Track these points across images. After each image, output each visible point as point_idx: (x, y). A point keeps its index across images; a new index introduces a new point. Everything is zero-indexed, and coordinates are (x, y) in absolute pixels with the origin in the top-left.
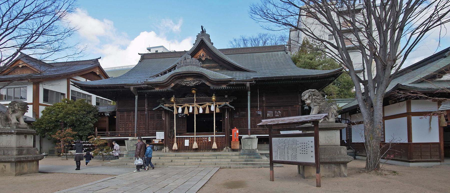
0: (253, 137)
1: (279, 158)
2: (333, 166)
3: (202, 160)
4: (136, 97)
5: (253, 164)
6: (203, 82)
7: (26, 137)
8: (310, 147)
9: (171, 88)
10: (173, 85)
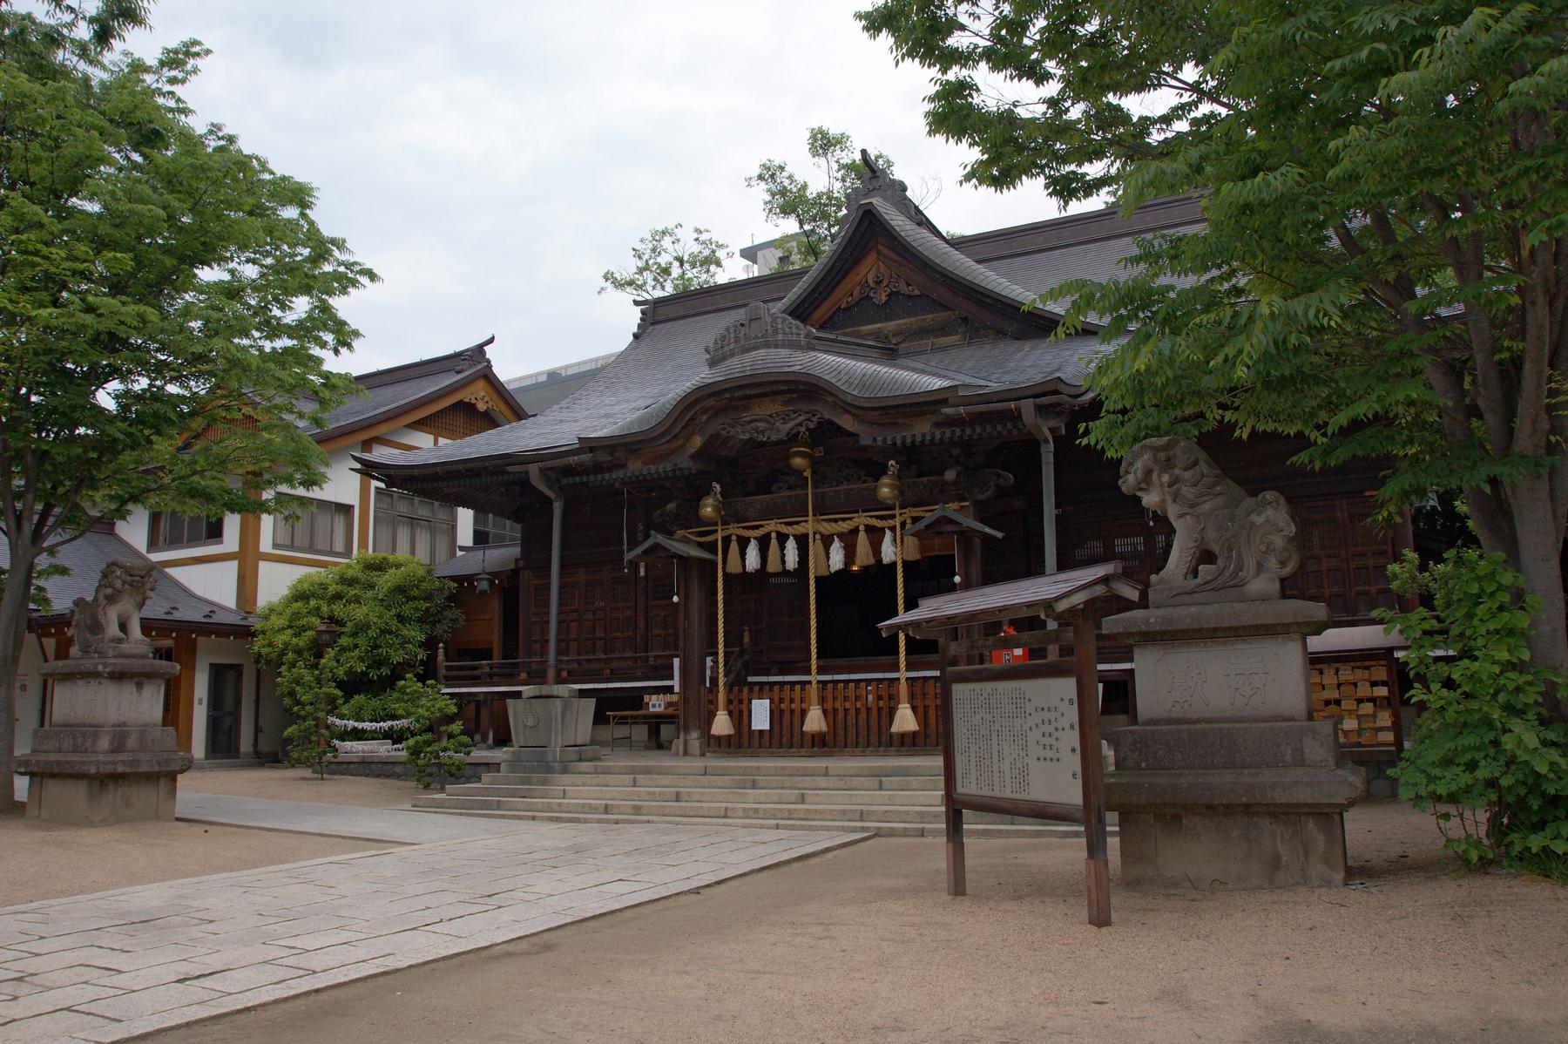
2: (1265, 823)
4: (557, 507)
6: (827, 416)
7: (140, 686)
8: (1067, 726)
9: (693, 457)
10: (697, 441)
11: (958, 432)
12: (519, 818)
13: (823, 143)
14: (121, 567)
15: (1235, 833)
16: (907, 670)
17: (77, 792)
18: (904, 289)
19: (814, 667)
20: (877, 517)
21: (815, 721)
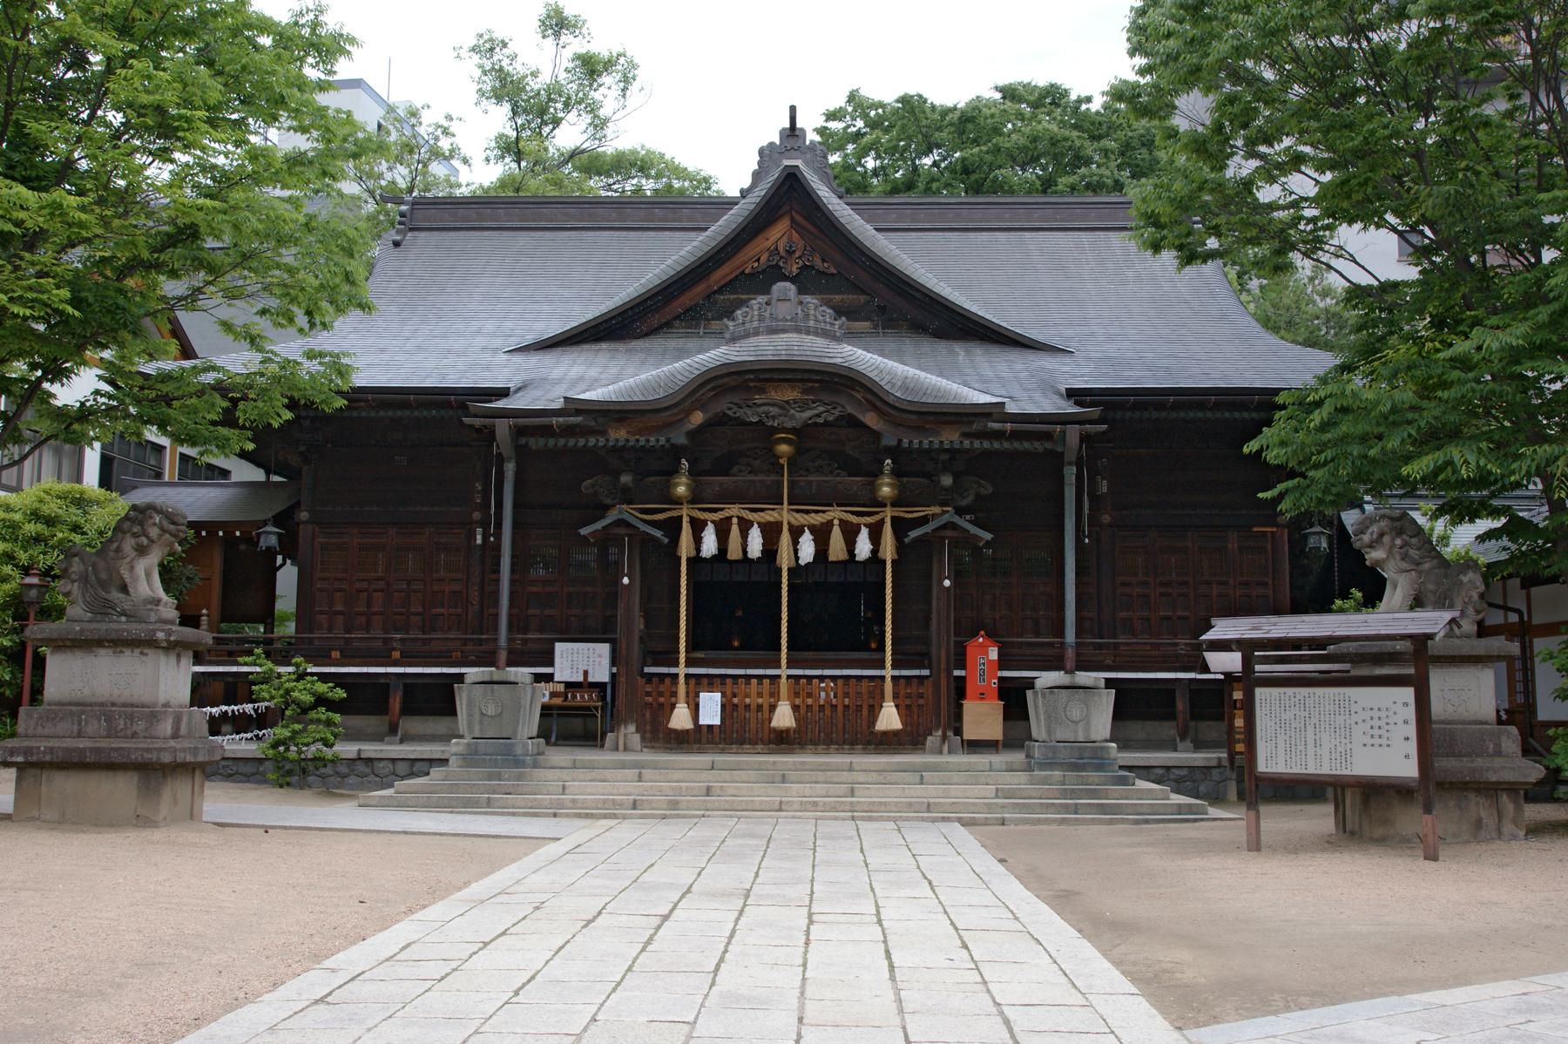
0: (1089, 683)
1: (1281, 760)
2: (1472, 796)
5: (1103, 809)
6: (850, 410)
7: (179, 656)
8: (1400, 722)
12: (514, 814)
13: (557, 24)
14: (159, 511)
15: (1452, 803)
17: (122, 788)
18: (818, 263)
19: (784, 662)
20: (853, 513)
21: (783, 717)
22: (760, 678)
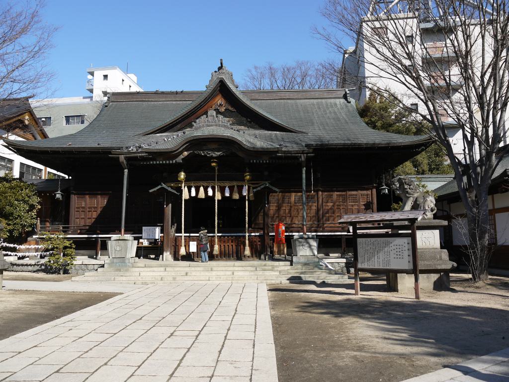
3: (235, 273)
9: (182, 159)
11: (274, 161)
16: (185, 233)
22: (228, 236)
